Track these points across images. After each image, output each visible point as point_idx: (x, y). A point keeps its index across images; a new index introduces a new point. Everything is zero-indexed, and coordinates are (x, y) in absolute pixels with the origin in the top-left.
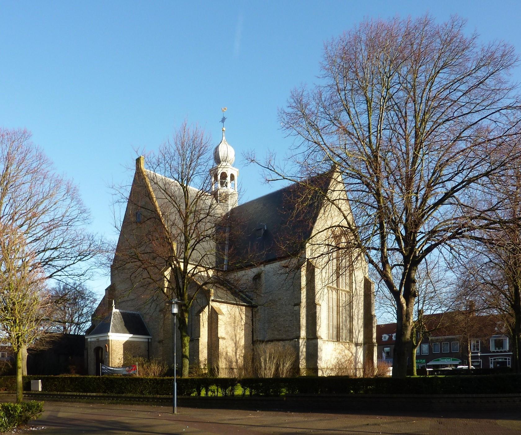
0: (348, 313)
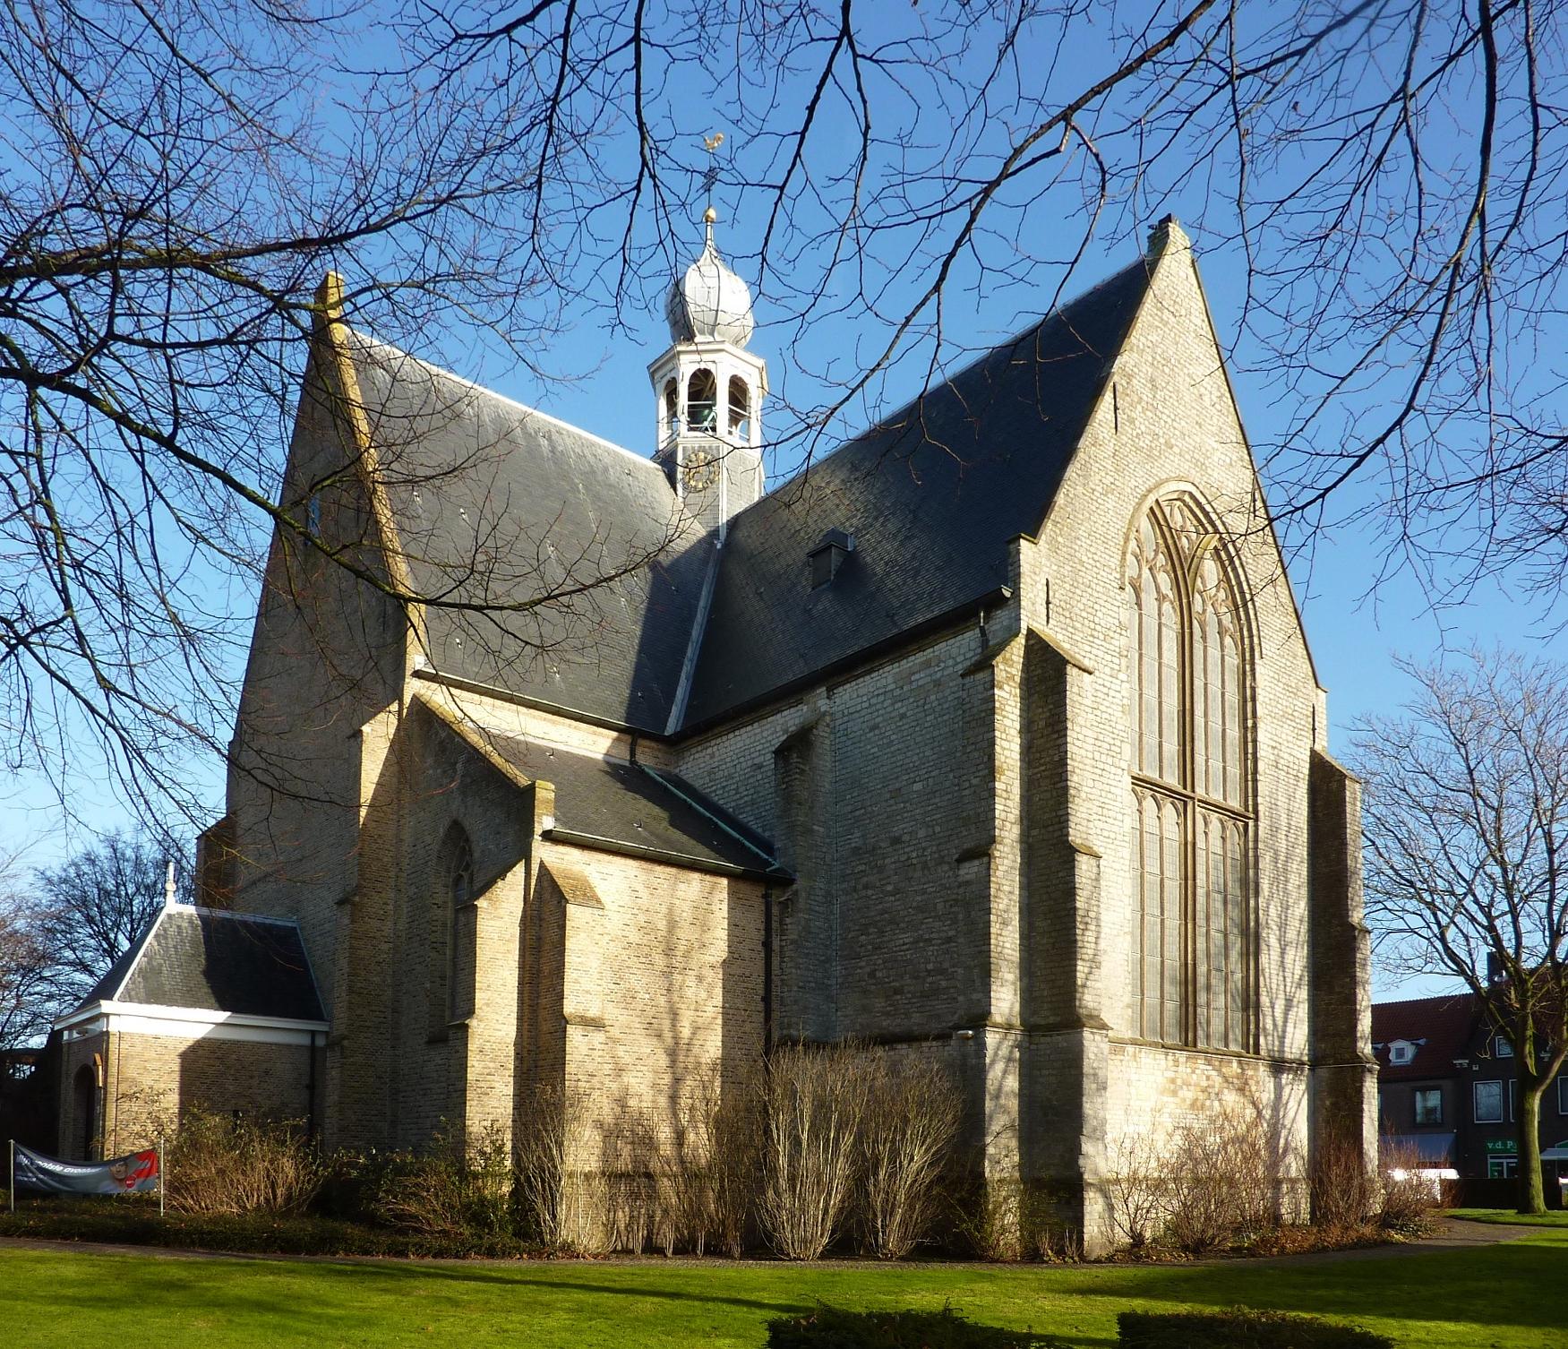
0: (1234, 913)
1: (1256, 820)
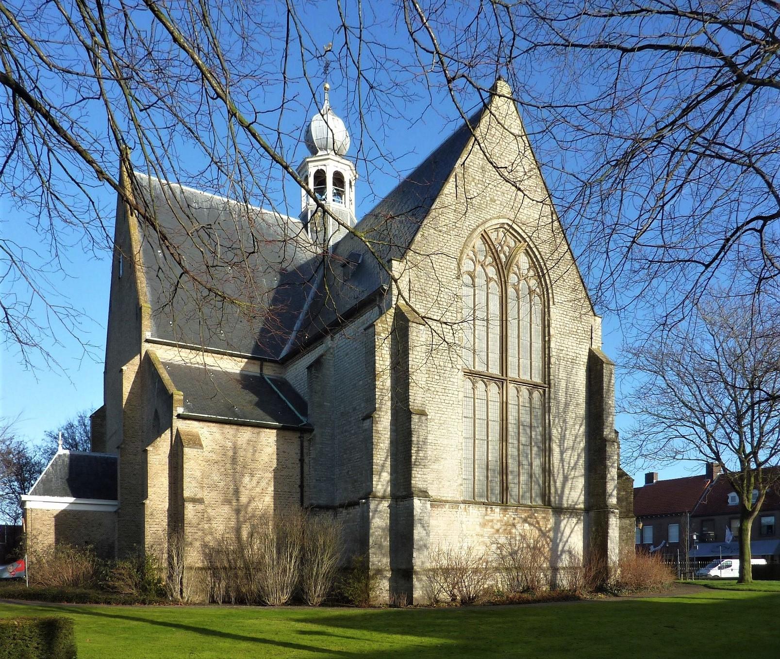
1: (549, 388)
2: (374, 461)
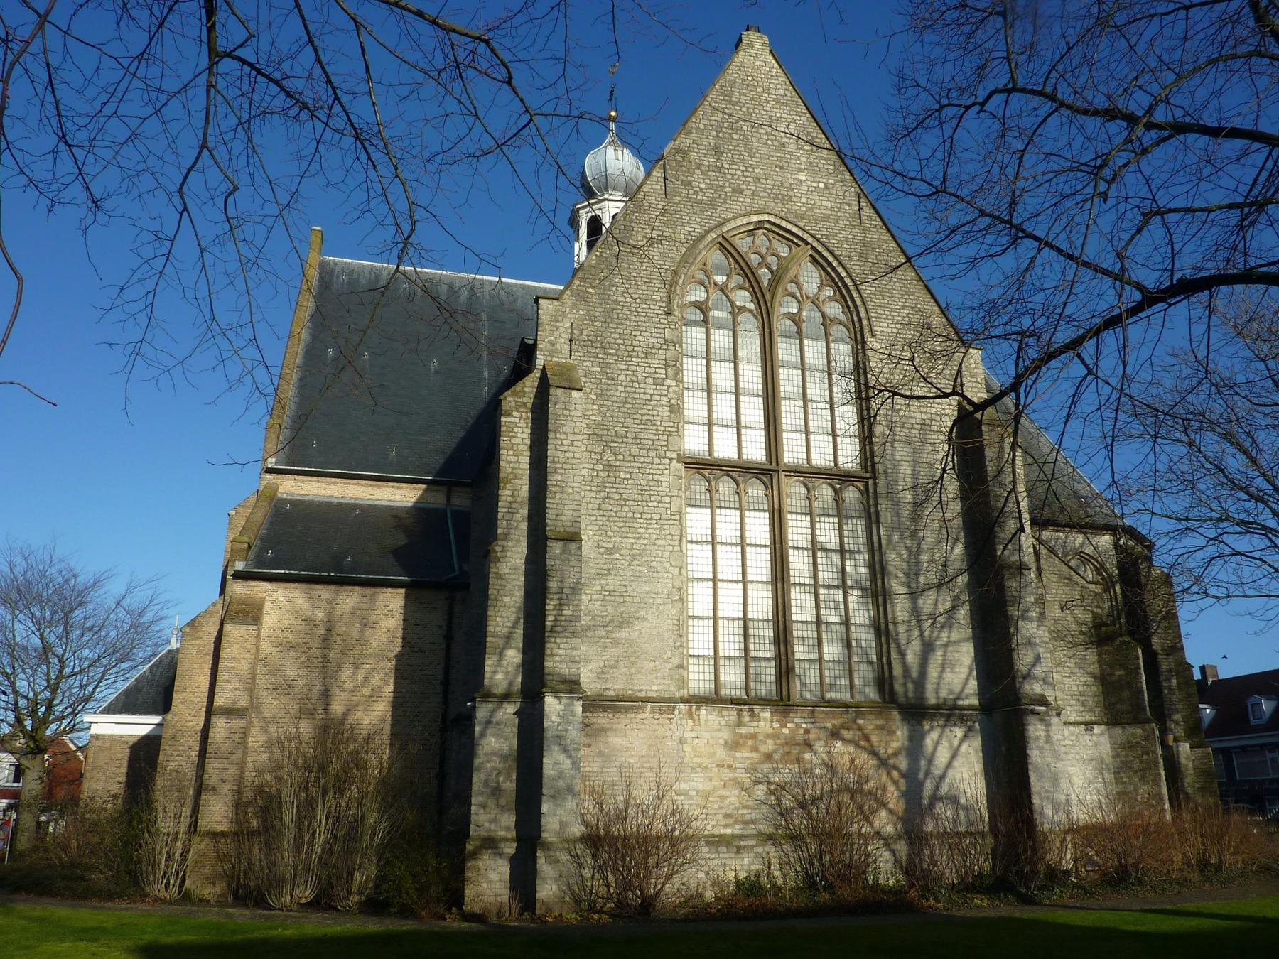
1: (875, 478)
2: (490, 628)
